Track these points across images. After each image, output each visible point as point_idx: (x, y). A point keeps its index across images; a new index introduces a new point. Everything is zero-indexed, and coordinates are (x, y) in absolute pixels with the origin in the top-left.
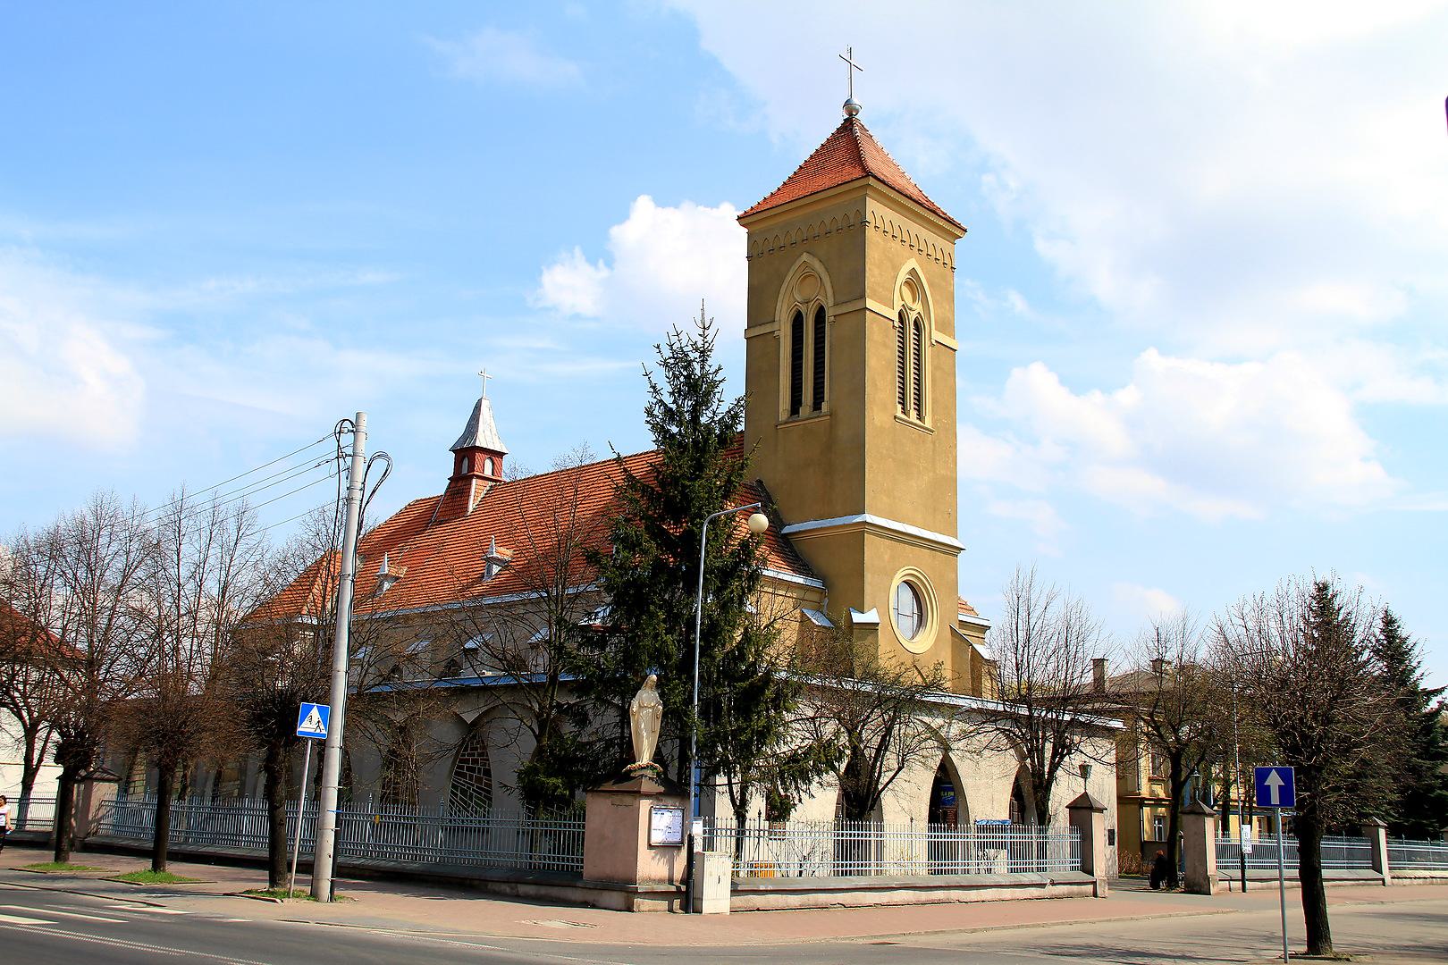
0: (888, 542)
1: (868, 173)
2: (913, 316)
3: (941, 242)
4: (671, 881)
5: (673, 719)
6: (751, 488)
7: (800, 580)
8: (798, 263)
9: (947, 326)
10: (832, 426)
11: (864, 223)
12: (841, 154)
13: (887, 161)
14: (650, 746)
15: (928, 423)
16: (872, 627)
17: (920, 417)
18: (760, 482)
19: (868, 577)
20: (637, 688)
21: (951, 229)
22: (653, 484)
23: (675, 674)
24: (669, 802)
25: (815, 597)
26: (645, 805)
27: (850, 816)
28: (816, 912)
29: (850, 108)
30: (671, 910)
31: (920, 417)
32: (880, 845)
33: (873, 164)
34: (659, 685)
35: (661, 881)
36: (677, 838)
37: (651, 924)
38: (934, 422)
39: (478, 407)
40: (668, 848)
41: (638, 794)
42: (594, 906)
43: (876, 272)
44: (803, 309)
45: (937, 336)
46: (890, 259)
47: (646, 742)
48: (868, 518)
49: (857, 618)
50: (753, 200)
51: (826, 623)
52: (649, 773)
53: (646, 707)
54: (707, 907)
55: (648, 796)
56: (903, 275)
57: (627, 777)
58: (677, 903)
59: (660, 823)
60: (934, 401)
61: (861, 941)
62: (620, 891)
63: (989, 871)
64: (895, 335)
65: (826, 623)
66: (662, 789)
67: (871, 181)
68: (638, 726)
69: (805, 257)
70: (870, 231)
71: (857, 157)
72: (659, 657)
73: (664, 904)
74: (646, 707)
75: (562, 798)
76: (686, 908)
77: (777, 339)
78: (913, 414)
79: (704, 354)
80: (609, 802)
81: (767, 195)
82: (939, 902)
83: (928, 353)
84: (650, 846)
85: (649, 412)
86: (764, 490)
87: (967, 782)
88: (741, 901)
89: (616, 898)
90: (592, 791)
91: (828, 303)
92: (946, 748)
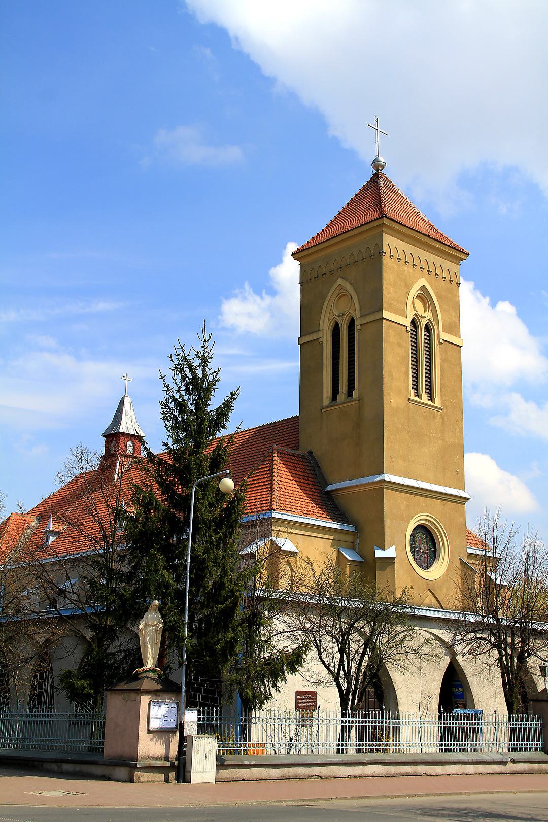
0: (404, 495)
1: (383, 215)
2: (424, 322)
3: (447, 264)
4: (167, 758)
5: (170, 635)
6: (303, 457)
7: (336, 526)
8: (335, 286)
9: (454, 328)
10: (360, 408)
11: (381, 253)
12: (368, 202)
13: (404, 203)
14: (153, 654)
15: (438, 403)
16: (390, 561)
17: (431, 398)
18: (310, 452)
19: (387, 522)
20: (146, 610)
21: (456, 254)
22: (167, 458)
23: (172, 604)
24: (166, 696)
25: (349, 538)
26: (145, 700)
27: (445, 711)
28: (298, 782)
29: (377, 166)
30: (167, 781)
31: (431, 398)
32: (397, 730)
33: (390, 209)
34: (160, 609)
35: (158, 758)
36: (173, 724)
37: (148, 791)
38: (443, 402)
39: (123, 399)
40: (162, 733)
41: (140, 692)
42: (109, 779)
43: (392, 290)
44: (339, 320)
45: (444, 336)
46: (404, 282)
47: (150, 652)
48: (387, 477)
49: (379, 553)
50: (306, 239)
51: (359, 559)
52: (151, 675)
53: (150, 627)
54: (195, 778)
55: (147, 692)
56: (414, 291)
57: (136, 678)
58: (172, 775)
59: (158, 713)
60: (443, 386)
61: (284, 804)
62: (125, 766)
63: (396, 751)
64: (409, 338)
65: (359, 559)
66: (160, 687)
67: (385, 221)
68: (144, 639)
69: (340, 281)
70: (386, 260)
71: (378, 203)
72: (163, 591)
73: (161, 776)
74: (150, 627)
75: (88, 696)
76: (178, 779)
77: (321, 344)
78: (425, 398)
79: (205, 361)
80: (121, 698)
81: (315, 235)
82: (407, 775)
83: (437, 349)
84: (149, 731)
85: (164, 405)
86: (313, 458)
87: (473, 682)
88: (226, 773)
89: (122, 772)
90: (111, 690)
91: (357, 315)
92: (453, 655)
